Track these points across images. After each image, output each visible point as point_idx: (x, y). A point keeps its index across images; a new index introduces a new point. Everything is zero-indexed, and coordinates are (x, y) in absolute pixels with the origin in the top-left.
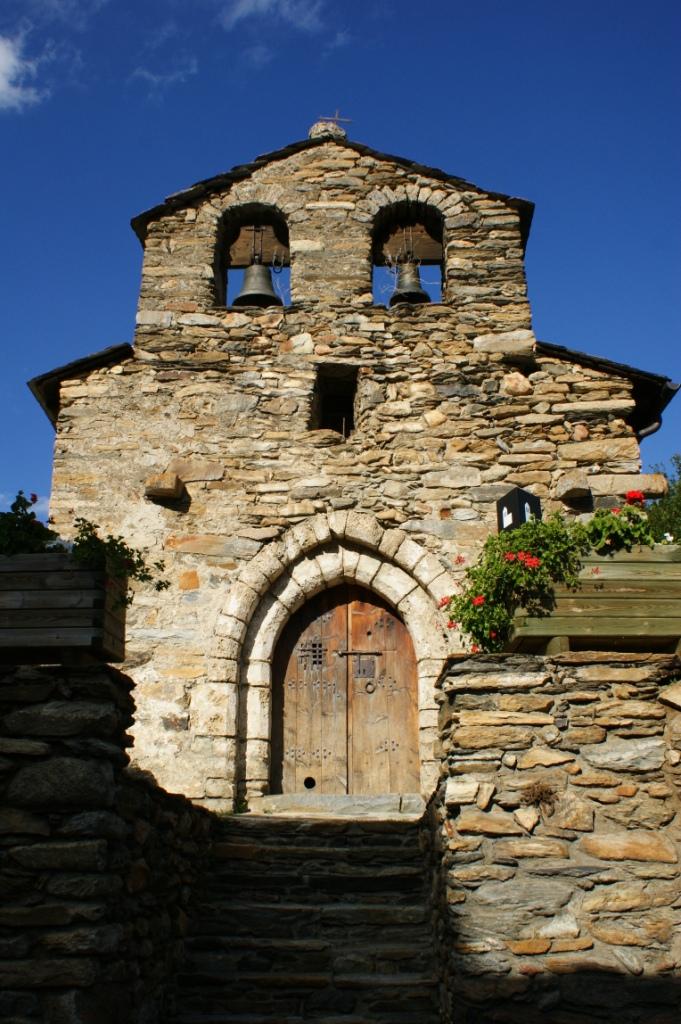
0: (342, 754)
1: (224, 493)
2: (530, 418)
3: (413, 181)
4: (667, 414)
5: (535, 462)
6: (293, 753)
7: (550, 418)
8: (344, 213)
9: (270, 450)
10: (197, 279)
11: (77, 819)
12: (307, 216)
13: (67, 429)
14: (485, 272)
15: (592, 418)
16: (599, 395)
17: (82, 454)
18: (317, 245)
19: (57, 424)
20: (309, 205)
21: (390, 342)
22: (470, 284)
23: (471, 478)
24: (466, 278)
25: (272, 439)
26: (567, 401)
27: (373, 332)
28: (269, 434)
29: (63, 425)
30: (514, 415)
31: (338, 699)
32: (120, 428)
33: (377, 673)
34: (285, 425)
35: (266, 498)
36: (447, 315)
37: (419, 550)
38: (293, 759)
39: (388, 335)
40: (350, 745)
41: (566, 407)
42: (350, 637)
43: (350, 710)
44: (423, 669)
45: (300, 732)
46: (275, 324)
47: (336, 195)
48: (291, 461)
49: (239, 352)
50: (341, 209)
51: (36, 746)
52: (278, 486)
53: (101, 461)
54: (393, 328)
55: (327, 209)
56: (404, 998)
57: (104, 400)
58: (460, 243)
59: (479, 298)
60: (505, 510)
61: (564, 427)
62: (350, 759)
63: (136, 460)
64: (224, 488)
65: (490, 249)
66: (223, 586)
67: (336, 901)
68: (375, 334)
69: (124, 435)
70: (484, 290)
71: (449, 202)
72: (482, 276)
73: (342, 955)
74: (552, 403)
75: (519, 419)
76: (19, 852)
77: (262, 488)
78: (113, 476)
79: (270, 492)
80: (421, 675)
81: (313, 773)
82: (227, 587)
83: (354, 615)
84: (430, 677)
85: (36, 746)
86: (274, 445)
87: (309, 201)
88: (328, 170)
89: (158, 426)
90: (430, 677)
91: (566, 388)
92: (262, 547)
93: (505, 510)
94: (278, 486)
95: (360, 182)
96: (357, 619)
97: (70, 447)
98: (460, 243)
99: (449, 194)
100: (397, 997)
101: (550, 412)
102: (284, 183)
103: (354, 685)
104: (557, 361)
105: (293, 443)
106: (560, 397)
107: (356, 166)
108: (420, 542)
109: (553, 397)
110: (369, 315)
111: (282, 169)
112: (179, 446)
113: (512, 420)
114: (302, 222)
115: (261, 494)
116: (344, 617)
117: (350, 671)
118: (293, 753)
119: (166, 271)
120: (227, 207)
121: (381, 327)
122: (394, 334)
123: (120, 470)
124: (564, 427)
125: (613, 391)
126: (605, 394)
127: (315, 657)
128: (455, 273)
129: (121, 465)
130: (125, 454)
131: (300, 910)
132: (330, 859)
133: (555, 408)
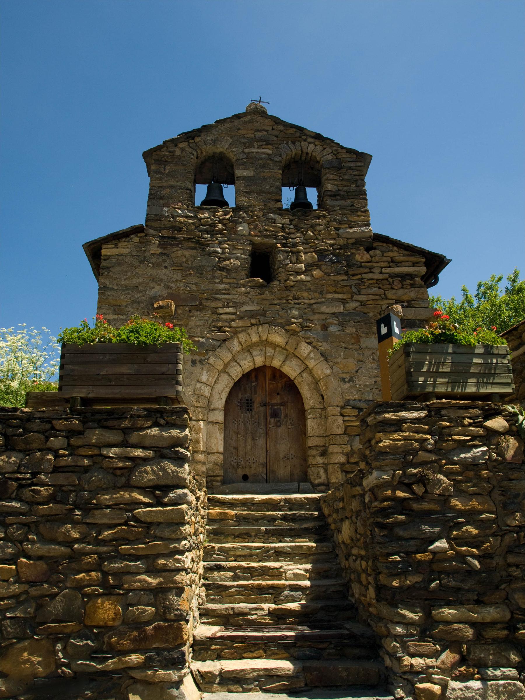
0: (263, 460)
1: (198, 313)
2: (370, 276)
3: (305, 140)
4: (441, 276)
5: (373, 300)
6: (235, 461)
7: (381, 277)
8: (266, 156)
9: (225, 290)
10: (182, 189)
11: (172, 493)
12: (245, 156)
13: (106, 273)
14: (345, 194)
15: (404, 277)
16: (407, 264)
17: (116, 288)
18: (251, 174)
19: (100, 271)
20: (247, 150)
21: (292, 230)
22: (336, 200)
23: (337, 308)
24: (334, 196)
25: (226, 283)
26: (390, 267)
27: (283, 224)
28: (225, 280)
29: (104, 271)
30: (361, 274)
31: (261, 431)
32: (138, 273)
33: (282, 416)
34: (234, 275)
35: (223, 317)
36: (324, 216)
37: (309, 348)
38: (236, 464)
39: (292, 227)
40: (268, 456)
41: (388, 270)
42: (267, 395)
43: (268, 439)
44: (310, 414)
45: (240, 449)
46: (228, 217)
47: (262, 145)
48: (238, 296)
49: (207, 232)
50: (265, 153)
51: (150, 454)
52: (231, 310)
53: (127, 292)
54: (294, 222)
55: (256, 153)
56: (329, 592)
57: (129, 257)
58: (331, 177)
59: (342, 208)
60: (382, 325)
61: (388, 281)
62: (268, 464)
63: (147, 292)
64: (199, 310)
65: (348, 180)
66: (199, 366)
67: (280, 542)
68: (284, 226)
69: (140, 278)
70: (343, 203)
71: (325, 152)
72: (343, 195)
73: (291, 570)
74: (382, 268)
75: (364, 276)
76: (139, 512)
77: (221, 311)
78: (137, 302)
79: (225, 313)
80: (309, 417)
81: (247, 472)
82: (201, 366)
83: (269, 384)
84: (314, 418)
85: (150, 454)
86: (227, 286)
87: (246, 148)
88: (257, 131)
89: (161, 273)
90: (314, 418)
91: (389, 259)
92: (221, 344)
93: (382, 325)
94: (231, 310)
95: (275, 139)
96: (271, 386)
97: (108, 284)
98: (331, 177)
99: (324, 149)
100: (325, 591)
101: (381, 273)
102: (231, 136)
103: (270, 422)
104: (385, 245)
105: (239, 285)
106: (386, 264)
107: (273, 129)
108: (310, 343)
109: (382, 265)
110: (280, 215)
111: (230, 128)
112: (173, 285)
113: (359, 277)
114: (242, 159)
115: (221, 314)
116: (264, 385)
117: (268, 415)
118: (235, 461)
119: (164, 184)
120: (218, 151)
121: (288, 222)
122: (295, 227)
123: (138, 298)
124: (388, 281)
125: (414, 264)
126: (410, 264)
127: (248, 406)
128: (329, 193)
129: (139, 295)
130: (141, 288)
131: (263, 547)
132: (273, 519)
133: (384, 271)
